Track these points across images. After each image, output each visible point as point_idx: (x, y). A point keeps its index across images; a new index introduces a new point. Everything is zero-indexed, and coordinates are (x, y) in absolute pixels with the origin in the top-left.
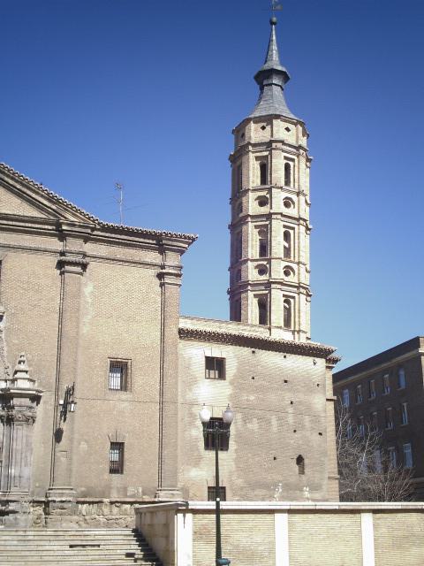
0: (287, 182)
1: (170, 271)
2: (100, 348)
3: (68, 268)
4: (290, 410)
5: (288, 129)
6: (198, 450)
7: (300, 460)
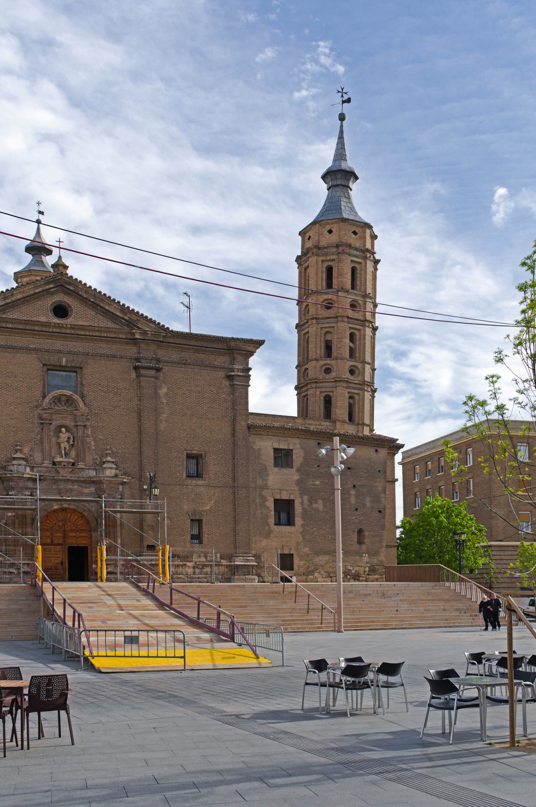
0: (353, 287)
1: (239, 374)
2: (176, 442)
3: (143, 372)
4: (353, 492)
5: (355, 233)
6: (268, 525)
7: (360, 532)
